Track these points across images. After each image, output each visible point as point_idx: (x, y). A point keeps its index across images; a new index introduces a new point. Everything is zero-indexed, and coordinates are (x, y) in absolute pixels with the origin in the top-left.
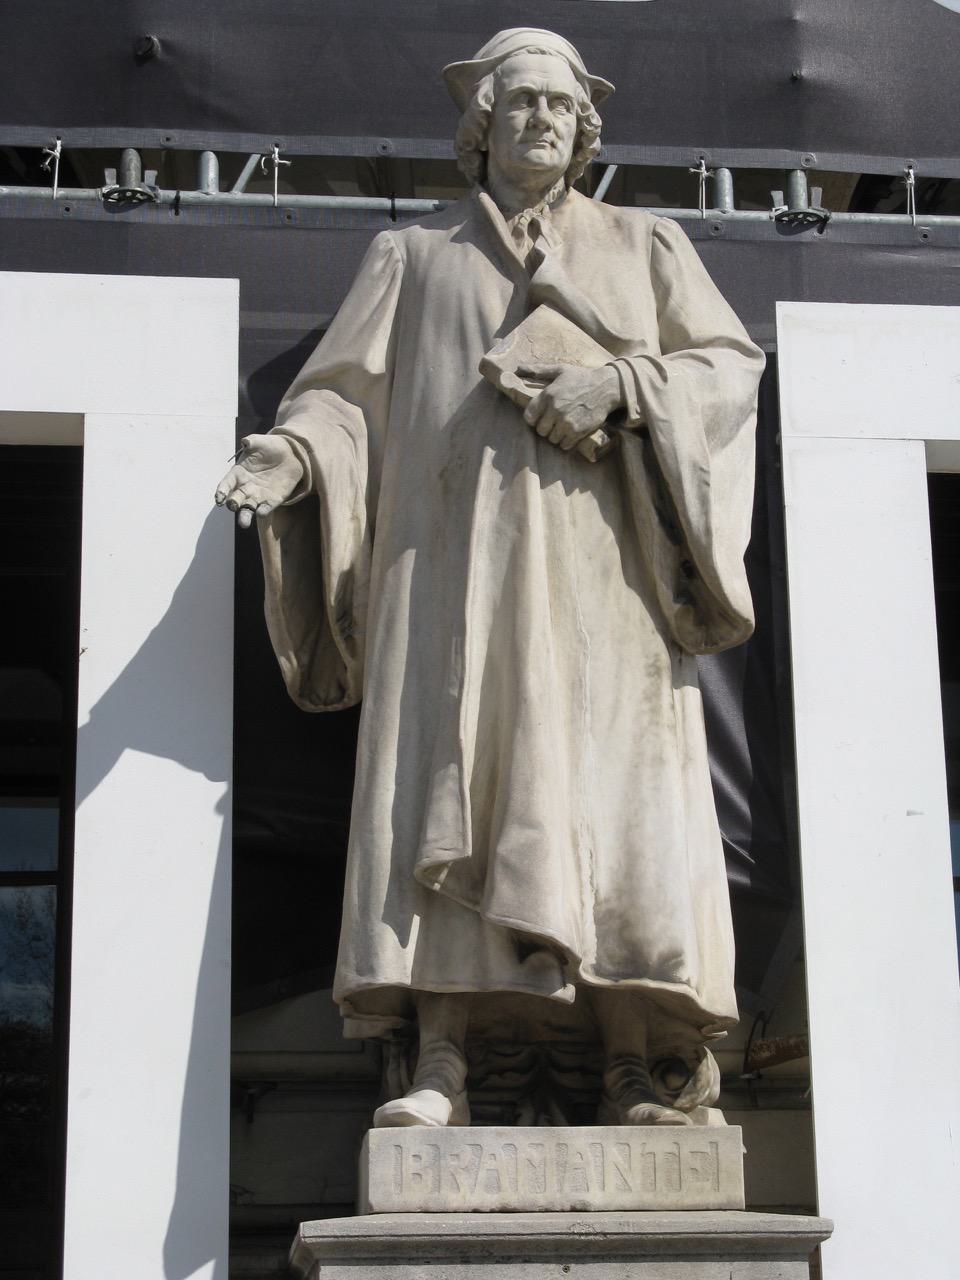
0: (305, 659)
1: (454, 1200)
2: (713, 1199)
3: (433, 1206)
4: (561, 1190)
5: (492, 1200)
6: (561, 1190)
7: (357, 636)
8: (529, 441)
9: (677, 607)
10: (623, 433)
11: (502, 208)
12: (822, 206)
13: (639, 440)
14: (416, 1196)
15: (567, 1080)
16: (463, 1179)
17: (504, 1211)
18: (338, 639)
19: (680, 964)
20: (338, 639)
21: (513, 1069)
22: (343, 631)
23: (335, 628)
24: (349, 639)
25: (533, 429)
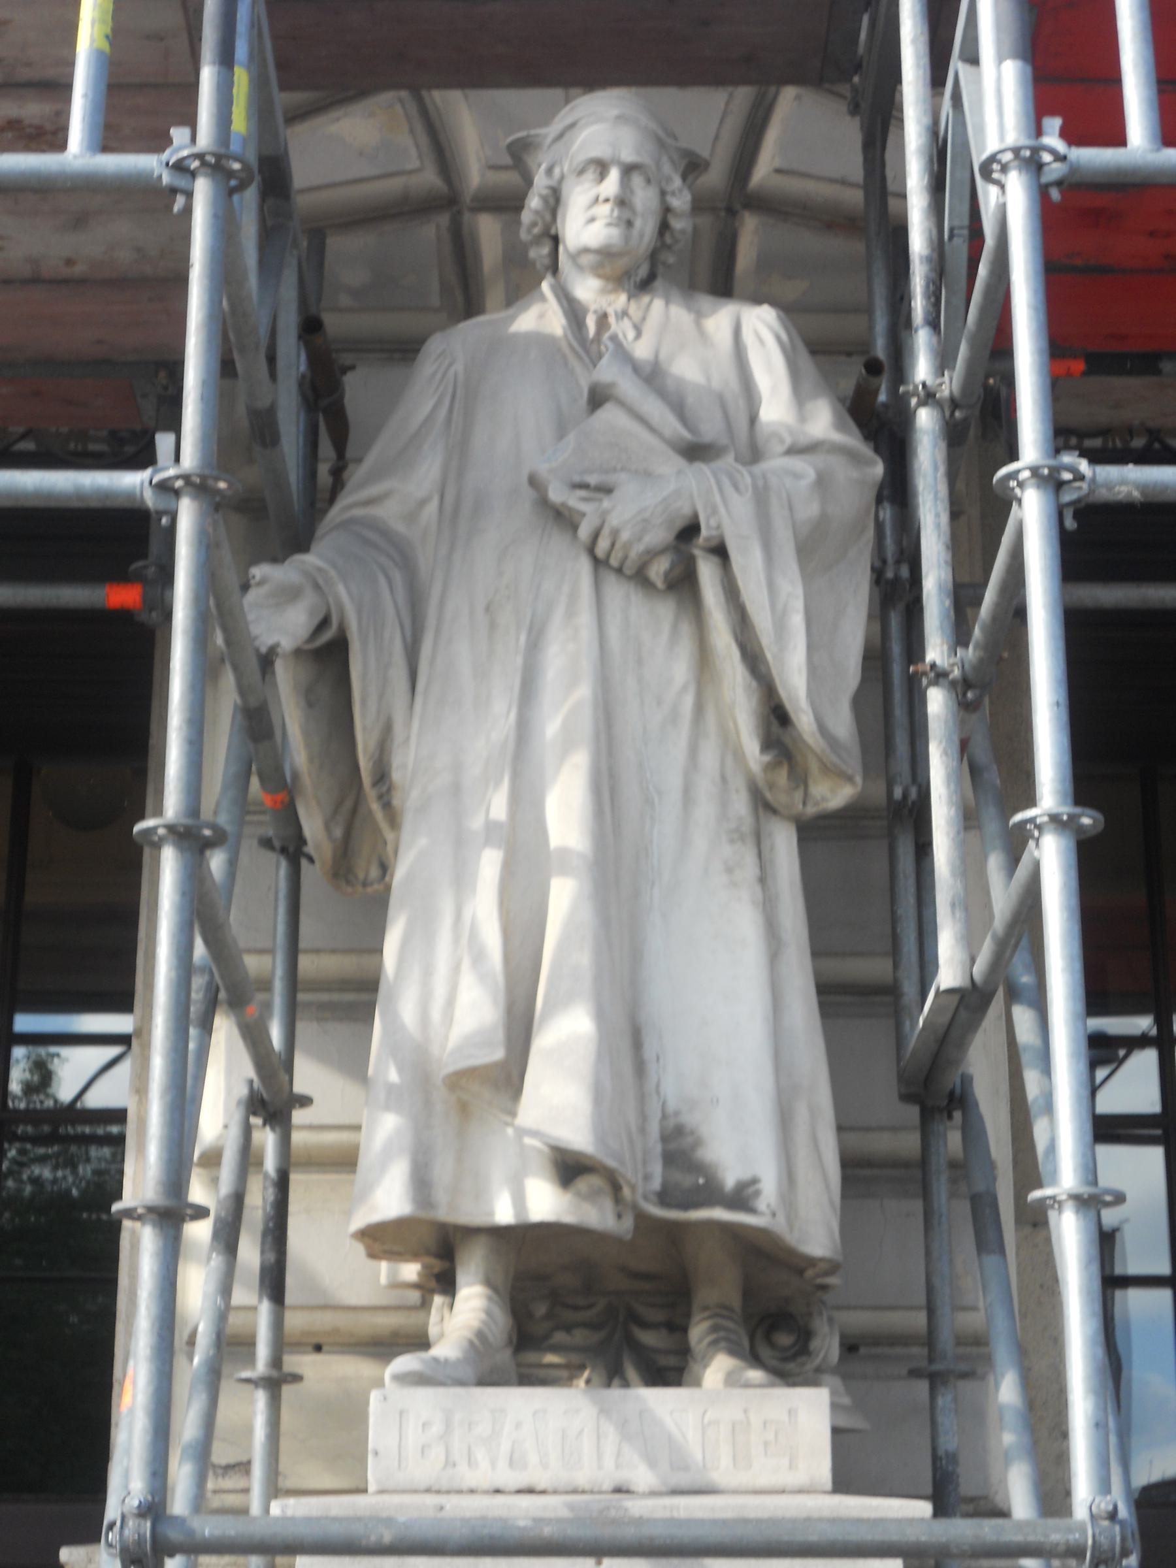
0: (338, 832)
1: (471, 1478)
2: (793, 1479)
3: (445, 1485)
4: (600, 1467)
5: (512, 1479)
6: (600, 1467)
7: (396, 802)
8: (585, 566)
9: (767, 758)
10: (697, 552)
11: (146, 1543)
12: (100, 1541)
13: (715, 560)
14: (424, 1471)
15: (649, 1338)
16: (480, 1455)
17: (531, 1491)
18: (375, 807)
19: (757, 1193)
20: (375, 807)
21: (585, 1325)
22: (380, 797)
23: (370, 792)
24: (387, 806)
25: (591, 550)
